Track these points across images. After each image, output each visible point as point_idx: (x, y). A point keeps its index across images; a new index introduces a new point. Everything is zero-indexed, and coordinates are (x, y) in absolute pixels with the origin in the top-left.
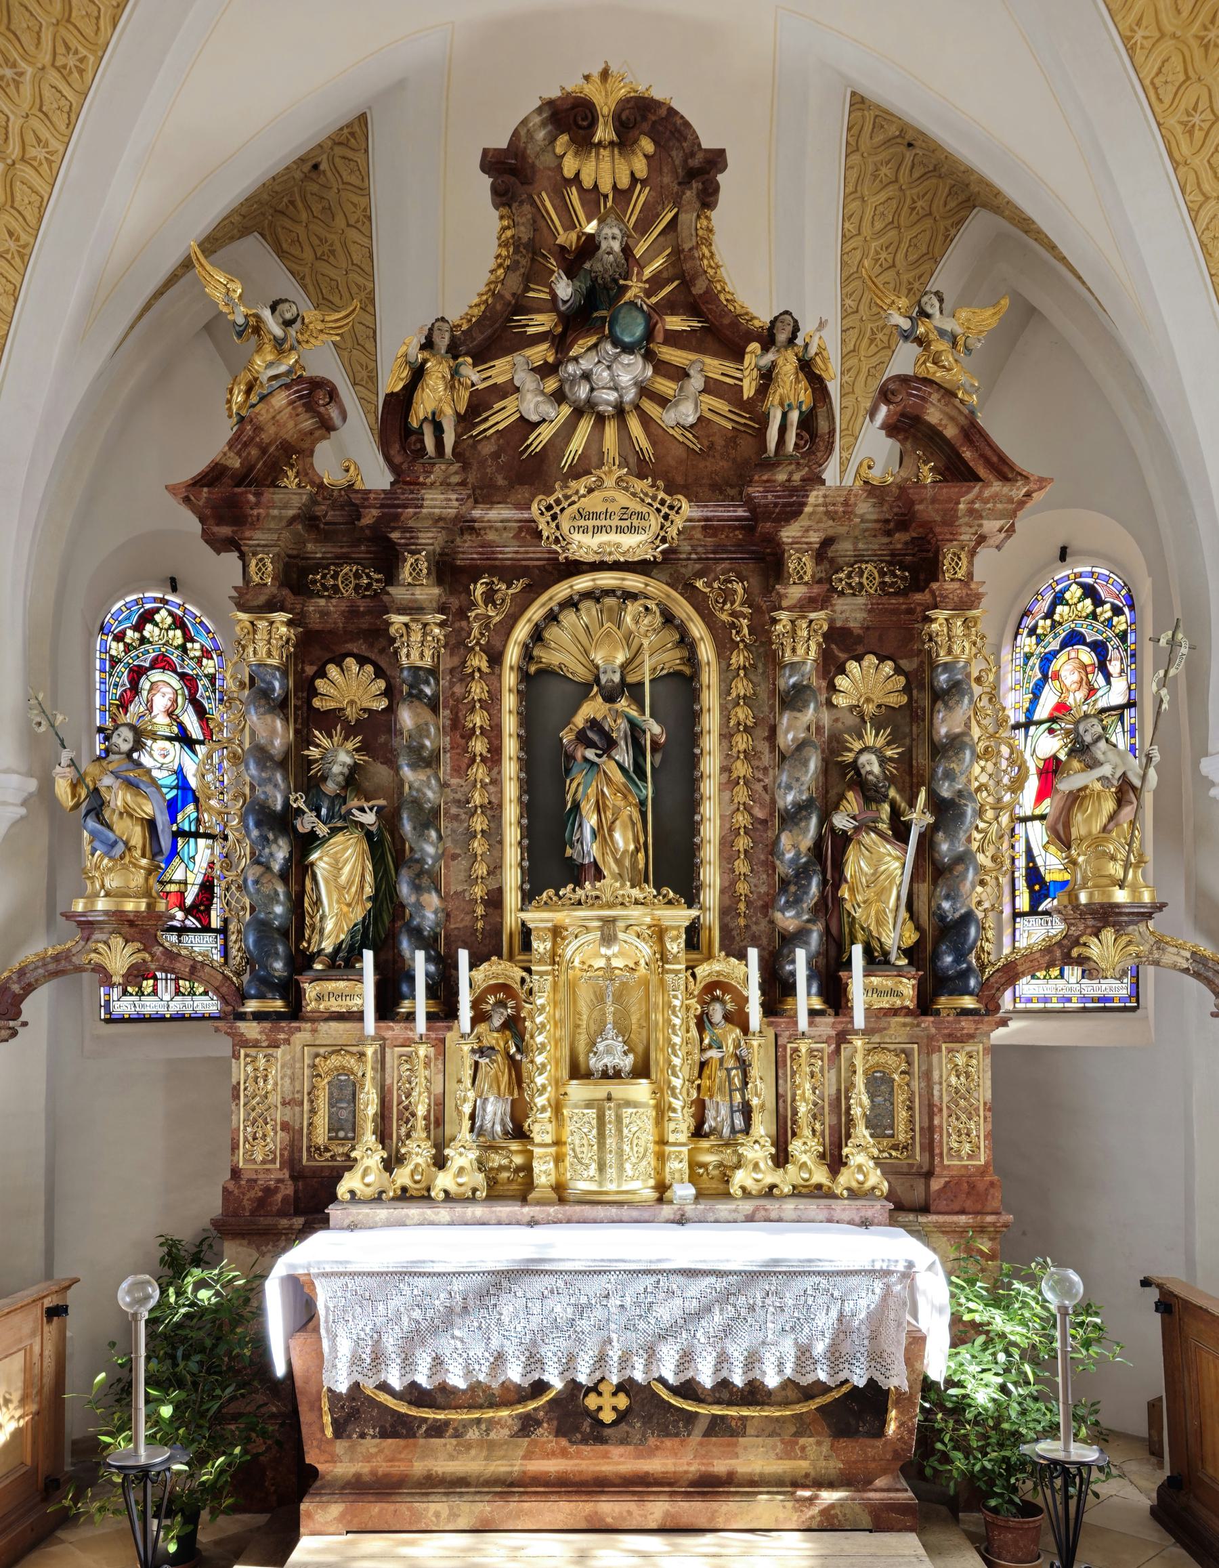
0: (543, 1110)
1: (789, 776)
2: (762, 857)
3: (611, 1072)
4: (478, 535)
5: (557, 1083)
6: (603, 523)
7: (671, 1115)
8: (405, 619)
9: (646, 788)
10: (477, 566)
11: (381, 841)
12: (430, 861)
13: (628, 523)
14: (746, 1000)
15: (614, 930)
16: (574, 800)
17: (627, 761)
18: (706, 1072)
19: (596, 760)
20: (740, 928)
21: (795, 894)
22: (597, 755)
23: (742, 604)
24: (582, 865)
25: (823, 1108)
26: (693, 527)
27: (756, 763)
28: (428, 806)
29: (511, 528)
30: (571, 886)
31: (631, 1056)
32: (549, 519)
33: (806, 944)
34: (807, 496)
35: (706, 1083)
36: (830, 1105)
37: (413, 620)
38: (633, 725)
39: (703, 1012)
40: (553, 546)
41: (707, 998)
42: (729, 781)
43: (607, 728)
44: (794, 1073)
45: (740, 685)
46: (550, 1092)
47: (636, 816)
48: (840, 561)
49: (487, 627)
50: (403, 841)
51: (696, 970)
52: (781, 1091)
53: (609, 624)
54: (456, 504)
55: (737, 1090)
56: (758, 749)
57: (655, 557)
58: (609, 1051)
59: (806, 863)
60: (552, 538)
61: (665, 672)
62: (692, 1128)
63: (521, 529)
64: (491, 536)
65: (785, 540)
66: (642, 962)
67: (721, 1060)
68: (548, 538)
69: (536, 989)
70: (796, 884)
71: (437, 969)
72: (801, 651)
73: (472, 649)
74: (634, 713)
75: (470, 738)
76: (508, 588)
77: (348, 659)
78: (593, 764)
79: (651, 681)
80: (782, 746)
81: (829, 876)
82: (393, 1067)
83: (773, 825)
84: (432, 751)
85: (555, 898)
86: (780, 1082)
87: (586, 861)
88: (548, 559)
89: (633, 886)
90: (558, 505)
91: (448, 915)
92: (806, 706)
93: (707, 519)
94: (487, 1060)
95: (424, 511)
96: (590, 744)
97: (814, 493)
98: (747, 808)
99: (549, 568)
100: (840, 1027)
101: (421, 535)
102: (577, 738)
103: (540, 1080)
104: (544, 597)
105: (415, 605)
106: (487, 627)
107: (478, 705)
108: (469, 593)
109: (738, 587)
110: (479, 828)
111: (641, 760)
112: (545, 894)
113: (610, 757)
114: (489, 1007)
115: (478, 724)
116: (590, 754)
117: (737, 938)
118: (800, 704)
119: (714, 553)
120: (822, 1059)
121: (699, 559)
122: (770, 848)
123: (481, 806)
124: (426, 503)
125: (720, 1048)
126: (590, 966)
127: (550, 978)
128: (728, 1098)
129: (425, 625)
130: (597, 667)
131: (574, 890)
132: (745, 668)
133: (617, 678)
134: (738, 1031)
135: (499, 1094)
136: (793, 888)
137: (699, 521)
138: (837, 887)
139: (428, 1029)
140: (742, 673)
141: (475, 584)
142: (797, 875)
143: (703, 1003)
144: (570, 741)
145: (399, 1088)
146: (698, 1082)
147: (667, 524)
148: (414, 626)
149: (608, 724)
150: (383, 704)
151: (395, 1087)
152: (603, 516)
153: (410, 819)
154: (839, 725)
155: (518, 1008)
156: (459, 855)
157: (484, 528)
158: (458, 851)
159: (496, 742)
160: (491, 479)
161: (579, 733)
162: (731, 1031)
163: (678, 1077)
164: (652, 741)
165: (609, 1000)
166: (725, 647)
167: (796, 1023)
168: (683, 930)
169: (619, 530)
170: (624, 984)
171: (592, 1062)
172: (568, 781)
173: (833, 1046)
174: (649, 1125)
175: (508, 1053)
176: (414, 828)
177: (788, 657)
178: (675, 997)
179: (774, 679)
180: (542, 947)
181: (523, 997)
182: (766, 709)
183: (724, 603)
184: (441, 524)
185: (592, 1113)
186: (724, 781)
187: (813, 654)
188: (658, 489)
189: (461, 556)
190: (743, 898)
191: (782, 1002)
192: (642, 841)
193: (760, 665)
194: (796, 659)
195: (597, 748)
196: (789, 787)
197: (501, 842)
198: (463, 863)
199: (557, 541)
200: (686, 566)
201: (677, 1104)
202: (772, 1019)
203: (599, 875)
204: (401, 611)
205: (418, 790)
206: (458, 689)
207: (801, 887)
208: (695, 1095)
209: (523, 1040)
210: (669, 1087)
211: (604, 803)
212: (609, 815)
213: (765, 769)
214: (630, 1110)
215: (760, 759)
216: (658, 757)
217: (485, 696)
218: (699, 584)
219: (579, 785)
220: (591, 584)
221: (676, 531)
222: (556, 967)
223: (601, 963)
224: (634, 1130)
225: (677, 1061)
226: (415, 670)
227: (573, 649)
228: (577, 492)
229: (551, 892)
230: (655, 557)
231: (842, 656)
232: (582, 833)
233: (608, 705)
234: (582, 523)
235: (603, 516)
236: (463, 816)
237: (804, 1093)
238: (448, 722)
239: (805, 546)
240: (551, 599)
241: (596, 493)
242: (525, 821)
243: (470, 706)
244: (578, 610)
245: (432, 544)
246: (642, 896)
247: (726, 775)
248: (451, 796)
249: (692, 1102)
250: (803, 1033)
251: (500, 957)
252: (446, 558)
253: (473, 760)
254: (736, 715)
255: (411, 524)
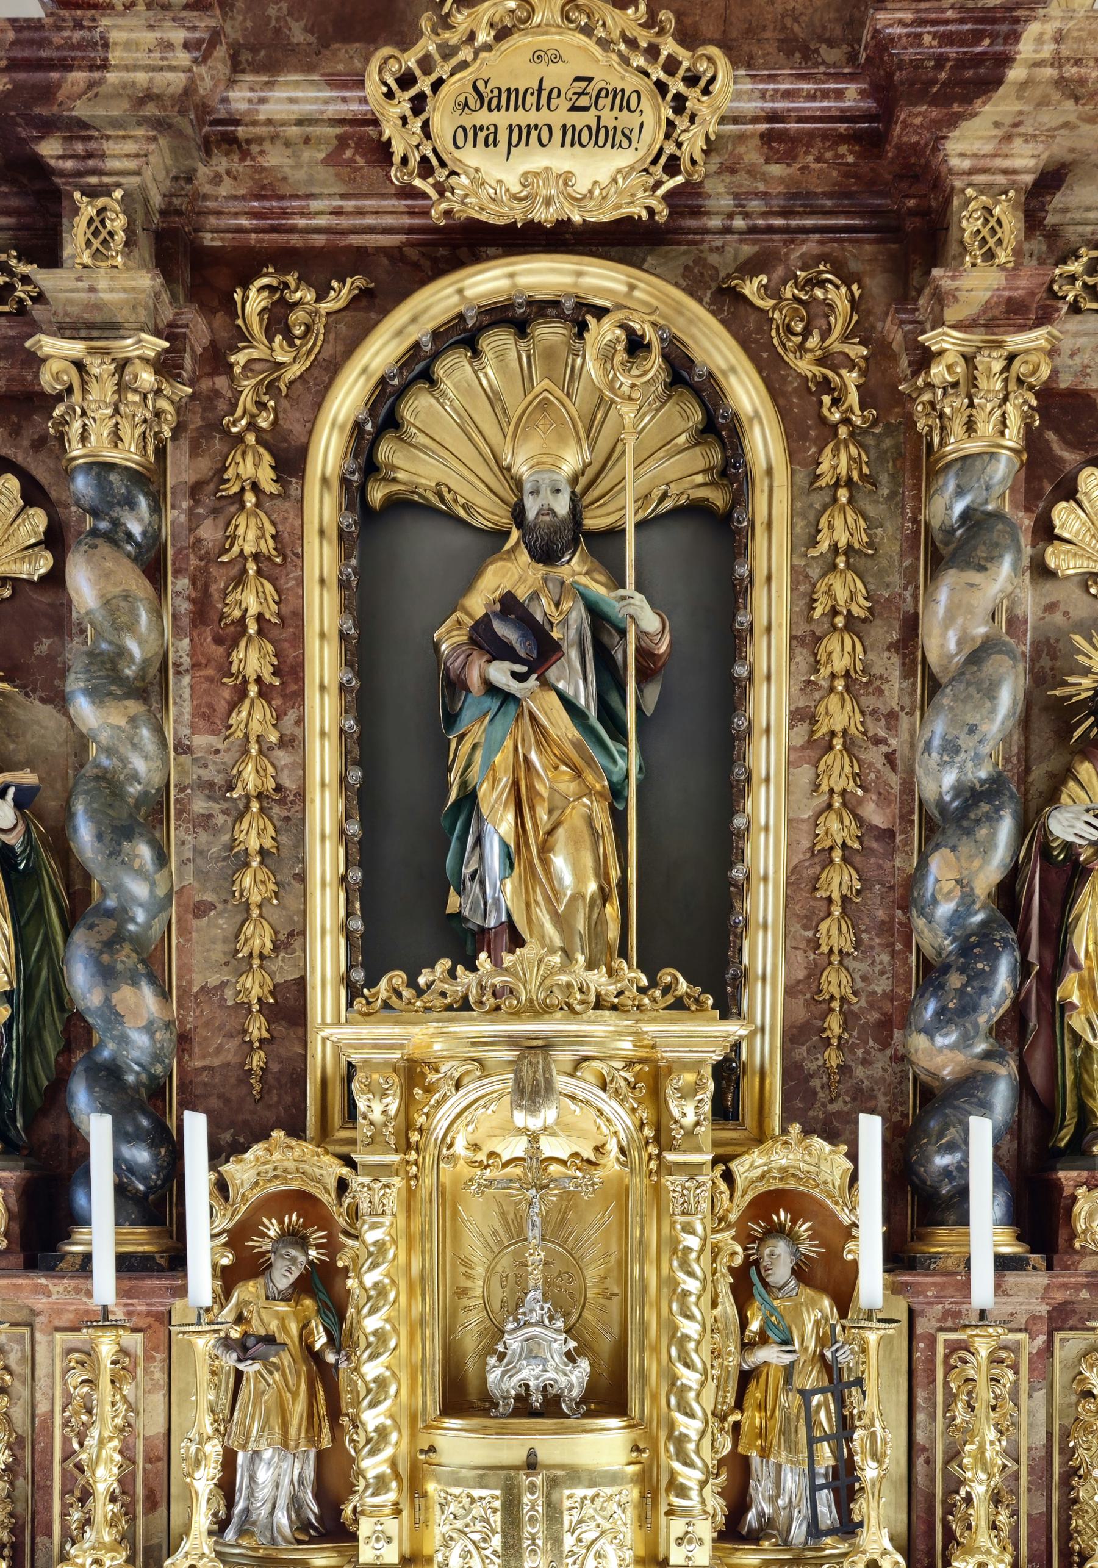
0: (380, 1485)
1: (953, 722)
2: (881, 914)
3: (537, 1401)
4: (245, 155)
5: (416, 1422)
6: (531, 117)
7: (676, 1501)
8: (76, 348)
9: (625, 755)
10: (251, 250)
11: (33, 874)
12: (141, 916)
13: (588, 118)
14: (849, 1232)
15: (547, 1069)
16: (464, 784)
17: (585, 696)
18: (755, 1393)
19: (514, 687)
20: (828, 1070)
21: (961, 992)
22: (514, 675)
23: (846, 339)
24: (483, 930)
25: (1016, 1476)
26: (742, 137)
27: (869, 702)
28: (134, 789)
29: (319, 140)
30: (445, 964)
31: (584, 1364)
32: (406, 108)
33: (984, 1108)
34: (1015, 37)
35: (752, 1418)
36: (1031, 1470)
37: (92, 352)
38: (597, 614)
39: (747, 1263)
40: (417, 182)
41: (757, 1229)
42: (810, 743)
43: (539, 618)
44: (951, 1399)
45: (838, 523)
46: (397, 1444)
47: (603, 820)
48: (1072, 233)
49: (271, 388)
50: (88, 878)
51: (733, 1165)
52: (920, 1437)
53: (546, 383)
54: (183, 58)
55: (826, 1438)
56: (877, 670)
57: (651, 211)
58: (532, 1352)
59: (984, 924)
60: (414, 159)
61: (668, 504)
62: (720, 1519)
63: (342, 142)
64: (274, 158)
65: (955, 162)
66: (612, 1147)
67: (789, 1370)
68: (405, 160)
69: (364, 1207)
70: (962, 970)
71: (156, 1157)
72: (987, 428)
73: (239, 438)
74: (598, 589)
75: (235, 644)
76: (319, 299)
77: (49, 556)
78: (507, 698)
79: (639, 525)
80: (933, 658)
81: (1033, 956)
82: (51, 1376)
83: (907, 842)
84: (146, 663)
85: (407, 993)
86: (920, 1417)
87: (492, 922)
88: (411, 230)
89: (591, 966)
90: (427, 72)
91: (184, 1040)
92: (994, 558)
93: (773, 117)
94: (257, 1366)
95: (112, 77)
96: (501, 651)
97: (1033, 29)
98: (850, 805)
99: (413, 254)
100: (1059, 1296)
101: (109, 147)
102: (472, 641)
103: (372, 1418)
104: (401, 315)
105: (98, 318)
106: (271, 388)
107: (252, 567)
108: (230, 309)
109: (839, 297)
110: (254, 844)
111: (614, 700)
112: (383, 984)
113: (545, 684)
114: (266, 1245)
115: (253, 610)
116: (500, 673)
117: (821, 1095)
118: (982, 552)
119: (785, 213)
120: (1015, 1368)
121: (753, 230)
122: (898, 892)
123: (260, 796)
124: (115, 56)
125: (785, 1342)
126: (492, 1154)
127: (397, 1181)
128: (803, 1456)
129: (122, 365)
130: (518, 484)
131: (452, 974)
132: (850, 483)
133: (562, 506)
134: (826, 1303)
135: (285, 1445)
136: (955, 980)
137: (755, 120)
138: (1051, 979)
139: (121, 1293)
140: (843, 495)
141: (246, 288)
142: (965, 950)
143: (746, 1238)
144: (455, 648)
145: (66, 1424)
146: (735, 1417)
147: (682, 123)
148: (98, 367)
149: (543, 609)
150: (44, 564)
151: (58, 1421)
152: (531, 100)
153: (93, 816)
154: (1058, 618)
155: (332, 1247)
156: (212, 907)
157: (260, 140)
158: (209, 897)
159: (292, 654)
160: (277, 31)
161: (475, 627)
162: (813, 1304)
163: (692, 1415)
164: (639, 650)
165: (534, 1235)
166: (804, 437)
167: (966, 1286)
168: (708, 1071)
169: (573, 137)
170: (568, 1196)
171: (493, 1377)
172: (453, 738)
173: (1043, 1338)
174: (626, 1524)
175: (309, 1348)
176: (99, 837)
177: (957, 444)
178: (689, 1229)
179: (917, 510)
180: (377, 1107)
181: (342, 1222)
182: (896, 579)
183: (806, 333)
184: (150, 110)
185: (492, 1495)
186: (799, 742)
187: (1013, 437)
188: (661, 32)
189: (213, 221)
190: (836, 1005)
191: (921, 1238)
192: (615, 874)
193: (884, 478)
194: (972, 447)
195: (515, 658)
196: (951, 748)
197: (302, 878)
198: (221, 924)
199: (426, 168)
200: (720, 250)
201: (690, 1477)
202: (905, 1278)
203: (517, 941)
204: (67, 329)
205: (109, 751)
206: (209, 532)
207: (974, 976)
208: (729, 1446)
209: (342, 1318)
210: (670, 1437)
211: (531, 788)
212: (542, 814)
213: (892, 717)
214: (580, 1492)
215: (880, 692)
216: (653, 693)
217: (268, 546)
218: (751, 289)
219: (475, 747)
220: (504, 283)
221: (701, 143)
222: (413, 1156)
223: (517, 1147)
224: (589, 1537)
225: (689, 1378)
226: (102, 469)
227: (465, 451)
228: (472, 37)
229: (398, 977)
230: (651, 211)
231: (1070, 457)
232: (482, 859)
233: (541, 570)
234: (483, 117)
235: (531, 100)
236: (220, 820)
237: (982, 1449)
238: (185, 606)
239: (1001, 179)
240: (414, 320)
241: (516, 40)
242: (354, 828)
243: (234, 571)
244: (476, 353)
245: (137, 173)
246: (613, 989)
247: (803, 729)
248: (195, 773)
249: (721, 1463)
250: (983, 1314)
251: (296, 1130)
252: (177, 221)
253: (241, 693)
254: (829, 592)
255: (81, 110)
